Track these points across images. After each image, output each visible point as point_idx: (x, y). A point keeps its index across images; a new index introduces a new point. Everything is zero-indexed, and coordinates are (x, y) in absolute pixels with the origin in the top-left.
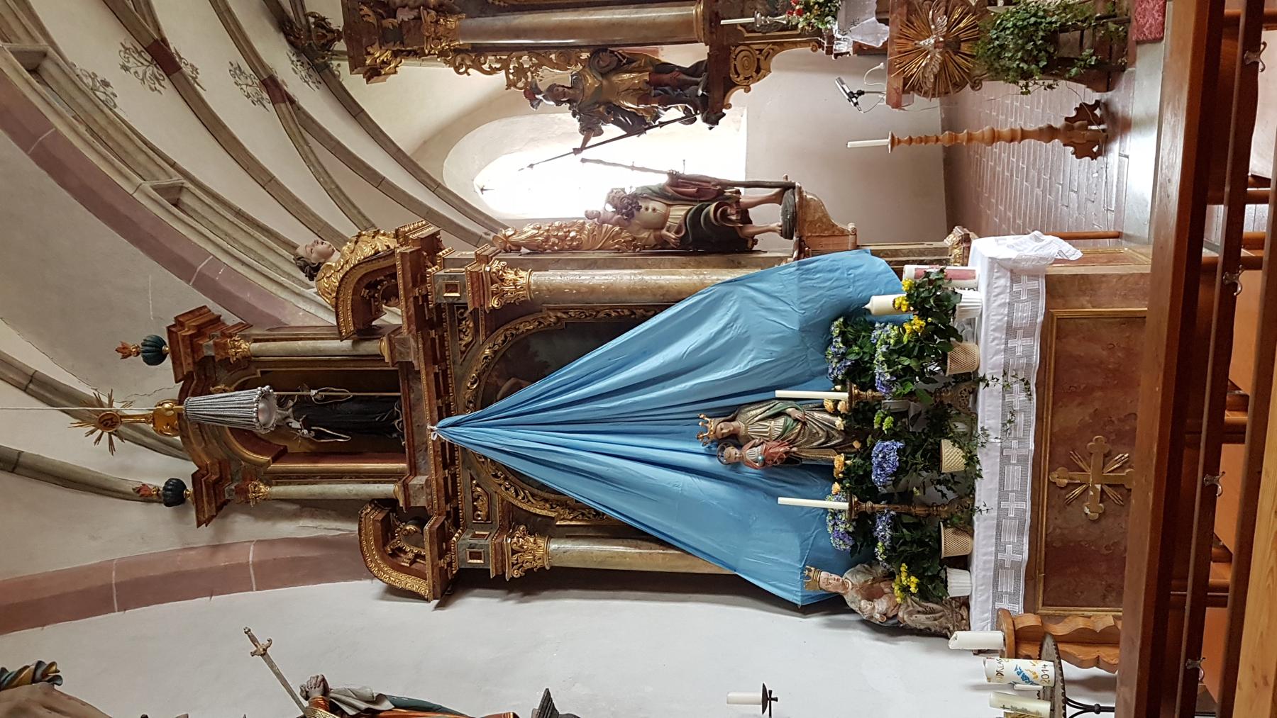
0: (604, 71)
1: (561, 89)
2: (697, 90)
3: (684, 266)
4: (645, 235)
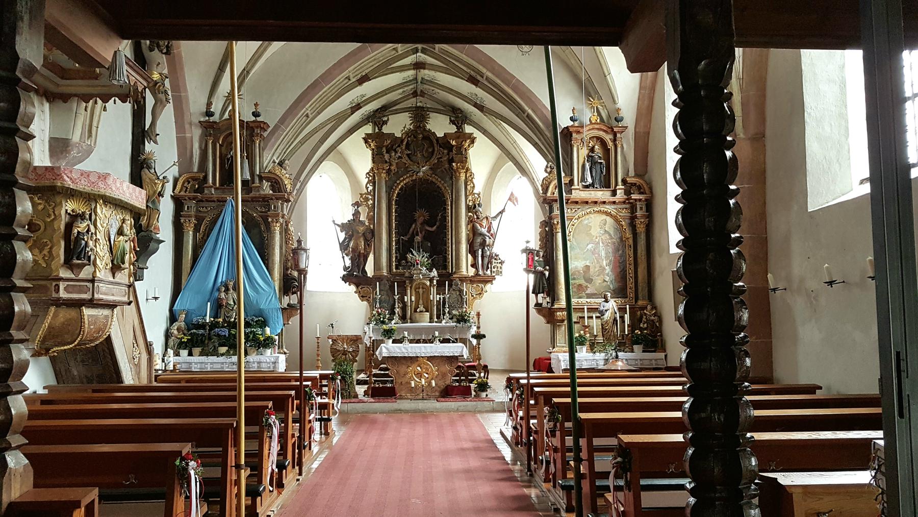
0: (365, 234)
2: (356, 272)
3: (280, 276)
4: (290, 264)
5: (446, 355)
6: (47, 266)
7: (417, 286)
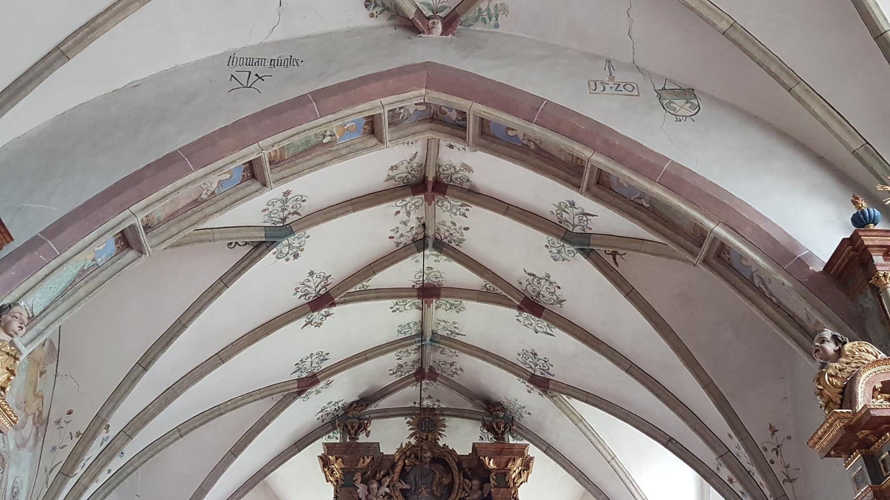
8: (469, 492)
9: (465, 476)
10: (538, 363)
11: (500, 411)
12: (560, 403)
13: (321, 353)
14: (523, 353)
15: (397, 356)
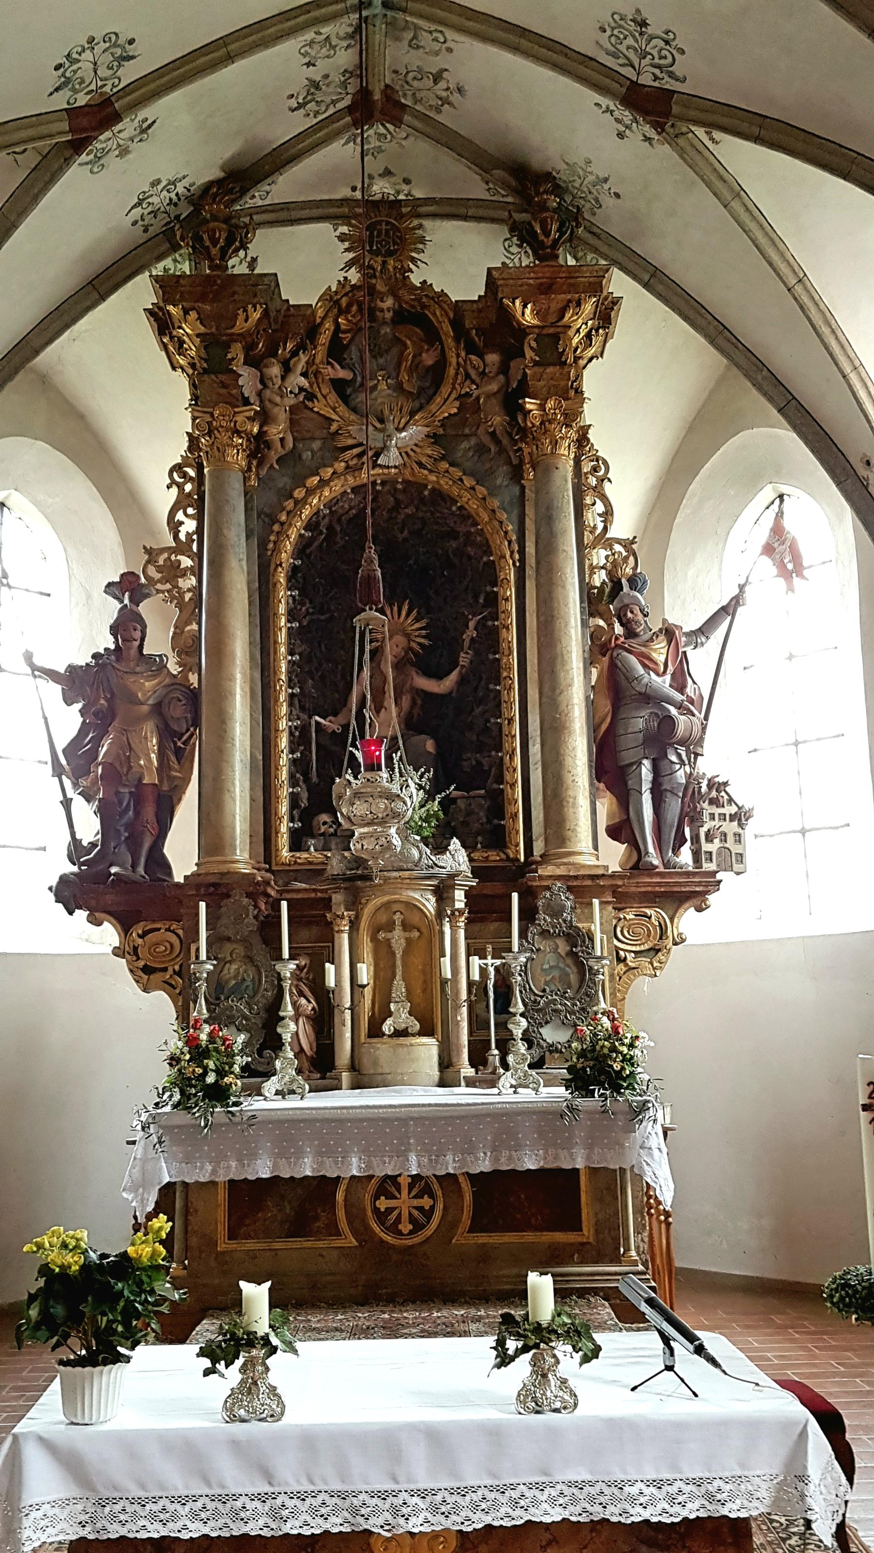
0: (165, 710)
1: (137, 635)
5: (638, 1515)
6: (419, 931)
7: (383, 918)
8: (478, 381)
9: (471, 349)
10: (647, 50)
11: (552, 193)
12: (692, 153)
13: (113, 38)
14: (613, 24)
15: (304, 55)
